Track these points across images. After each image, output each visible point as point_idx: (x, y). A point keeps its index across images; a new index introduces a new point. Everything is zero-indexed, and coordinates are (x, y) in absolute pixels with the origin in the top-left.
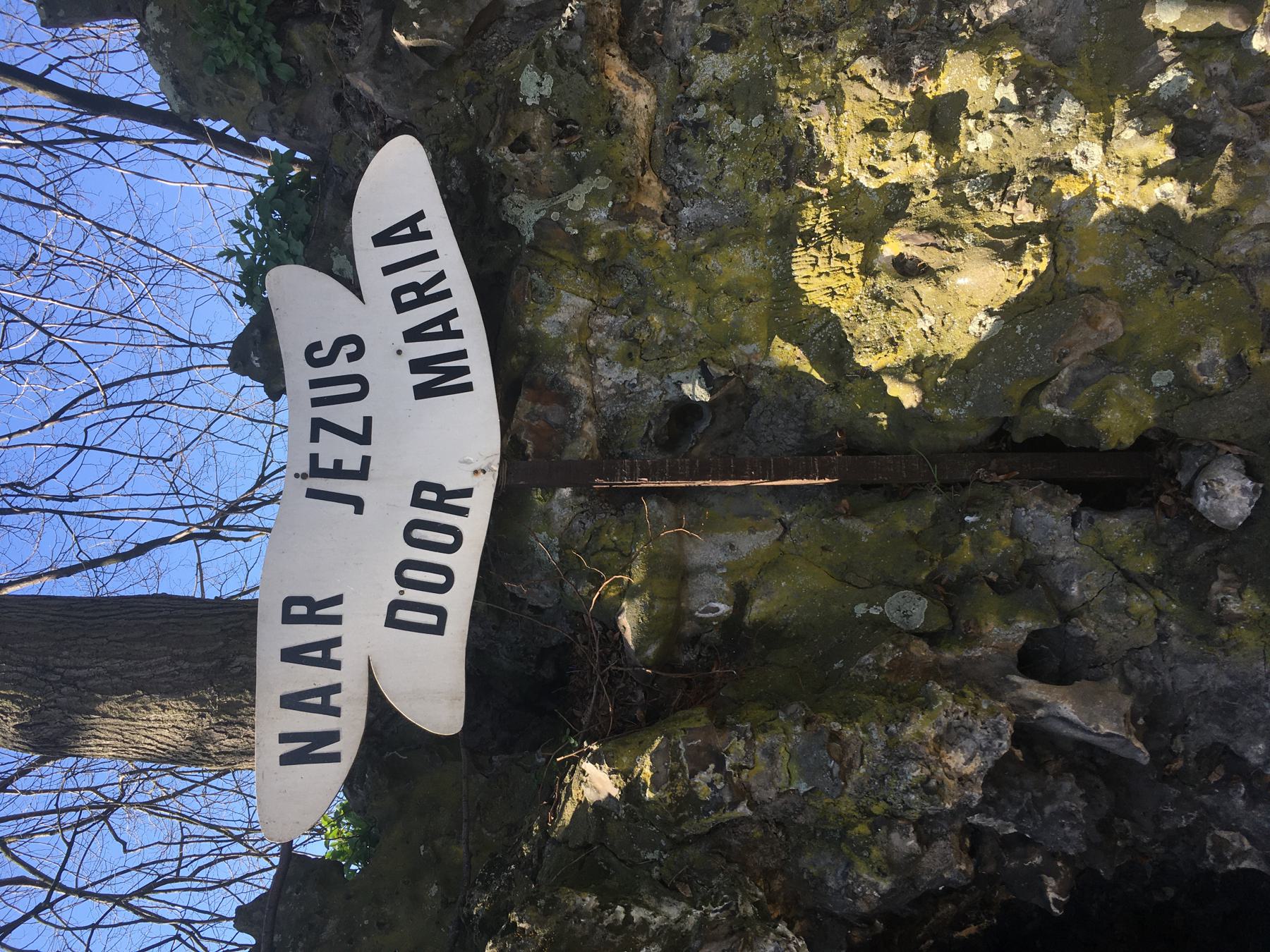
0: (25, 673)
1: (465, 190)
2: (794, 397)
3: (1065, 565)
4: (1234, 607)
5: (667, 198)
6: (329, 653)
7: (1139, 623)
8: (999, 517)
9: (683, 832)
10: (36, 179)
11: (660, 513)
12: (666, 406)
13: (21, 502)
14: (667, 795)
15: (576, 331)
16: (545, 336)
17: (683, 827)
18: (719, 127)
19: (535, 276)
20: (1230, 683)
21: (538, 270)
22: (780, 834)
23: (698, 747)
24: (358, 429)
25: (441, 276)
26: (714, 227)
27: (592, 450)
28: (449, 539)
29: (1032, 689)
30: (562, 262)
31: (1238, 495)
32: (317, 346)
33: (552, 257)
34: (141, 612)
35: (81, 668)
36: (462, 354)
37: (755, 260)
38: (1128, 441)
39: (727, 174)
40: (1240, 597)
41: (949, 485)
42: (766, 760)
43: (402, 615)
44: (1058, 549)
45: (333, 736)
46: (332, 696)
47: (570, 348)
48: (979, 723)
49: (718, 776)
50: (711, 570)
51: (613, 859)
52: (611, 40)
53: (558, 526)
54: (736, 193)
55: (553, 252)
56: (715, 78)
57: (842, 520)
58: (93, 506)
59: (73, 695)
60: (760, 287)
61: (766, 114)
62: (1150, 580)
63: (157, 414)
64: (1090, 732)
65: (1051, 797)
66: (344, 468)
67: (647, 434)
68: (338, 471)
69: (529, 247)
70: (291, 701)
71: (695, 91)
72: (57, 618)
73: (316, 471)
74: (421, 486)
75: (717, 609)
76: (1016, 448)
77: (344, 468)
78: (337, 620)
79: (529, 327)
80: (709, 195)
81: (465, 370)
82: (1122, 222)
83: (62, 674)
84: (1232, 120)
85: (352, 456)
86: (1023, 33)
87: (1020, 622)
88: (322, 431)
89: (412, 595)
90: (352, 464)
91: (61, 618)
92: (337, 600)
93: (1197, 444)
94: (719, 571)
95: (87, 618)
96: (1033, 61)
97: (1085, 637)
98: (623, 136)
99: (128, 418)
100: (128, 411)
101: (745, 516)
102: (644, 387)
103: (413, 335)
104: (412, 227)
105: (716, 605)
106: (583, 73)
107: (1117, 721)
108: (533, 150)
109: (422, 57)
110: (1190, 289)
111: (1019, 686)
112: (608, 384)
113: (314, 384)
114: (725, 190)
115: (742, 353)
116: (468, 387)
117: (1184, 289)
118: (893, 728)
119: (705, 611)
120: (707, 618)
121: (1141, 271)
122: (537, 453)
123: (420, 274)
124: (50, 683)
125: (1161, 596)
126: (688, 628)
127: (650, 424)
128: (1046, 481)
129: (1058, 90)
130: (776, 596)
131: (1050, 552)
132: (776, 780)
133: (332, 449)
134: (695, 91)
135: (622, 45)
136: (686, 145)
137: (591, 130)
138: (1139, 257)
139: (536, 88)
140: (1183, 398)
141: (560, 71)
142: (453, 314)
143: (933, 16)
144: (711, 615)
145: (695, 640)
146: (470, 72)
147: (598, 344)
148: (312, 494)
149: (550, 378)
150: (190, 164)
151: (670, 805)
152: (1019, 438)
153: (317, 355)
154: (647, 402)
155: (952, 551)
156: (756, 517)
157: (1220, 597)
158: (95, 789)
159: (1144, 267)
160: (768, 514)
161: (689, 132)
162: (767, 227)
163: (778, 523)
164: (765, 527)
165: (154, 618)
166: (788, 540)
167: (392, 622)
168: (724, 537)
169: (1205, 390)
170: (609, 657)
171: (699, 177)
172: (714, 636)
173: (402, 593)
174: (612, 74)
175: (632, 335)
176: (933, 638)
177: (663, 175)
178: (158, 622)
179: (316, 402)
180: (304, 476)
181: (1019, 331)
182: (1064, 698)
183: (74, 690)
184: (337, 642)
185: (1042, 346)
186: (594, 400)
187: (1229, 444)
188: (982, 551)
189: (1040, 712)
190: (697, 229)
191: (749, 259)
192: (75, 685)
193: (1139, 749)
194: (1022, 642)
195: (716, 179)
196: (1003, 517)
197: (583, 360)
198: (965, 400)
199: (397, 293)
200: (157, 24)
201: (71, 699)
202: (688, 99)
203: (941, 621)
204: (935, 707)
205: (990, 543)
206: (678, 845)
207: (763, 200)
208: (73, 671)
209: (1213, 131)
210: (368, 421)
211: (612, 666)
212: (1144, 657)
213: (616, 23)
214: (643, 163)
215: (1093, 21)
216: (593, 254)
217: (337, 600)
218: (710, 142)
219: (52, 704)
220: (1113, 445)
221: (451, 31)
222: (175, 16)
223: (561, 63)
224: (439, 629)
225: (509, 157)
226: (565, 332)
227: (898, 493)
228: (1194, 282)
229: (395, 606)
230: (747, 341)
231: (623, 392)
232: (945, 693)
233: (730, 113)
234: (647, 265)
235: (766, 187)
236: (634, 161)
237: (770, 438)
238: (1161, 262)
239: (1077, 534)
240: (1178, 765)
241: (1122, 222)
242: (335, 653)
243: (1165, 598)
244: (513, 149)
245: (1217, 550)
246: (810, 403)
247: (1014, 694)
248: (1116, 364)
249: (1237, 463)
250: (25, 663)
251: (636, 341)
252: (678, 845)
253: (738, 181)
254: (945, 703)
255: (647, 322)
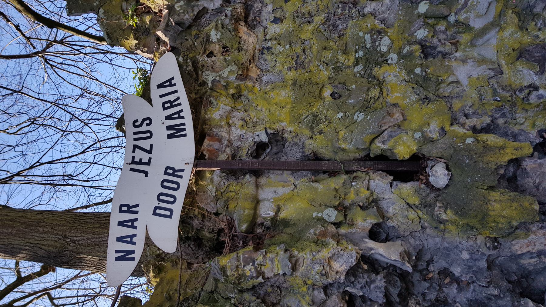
0: (58, 238)
1: (192, 70)
2: (299, 141)
3: (387, 201)
4: (444, 217)
5: (259, 73)
6: (133, 224)
7: (413, 222)
8: (363, 183)
9: (242, 287)
10: (82, 65)
11: (250, 180)
12: (255, 143)
13: (70, 182)
14: (236, 273)
15: (225, 117)
16: (214, 119)
17: (242, 286)
18: (275, 49)
19: (212, 99)
20: (447, 245)
21: (213, 97)
22: (278, 291)
23: (247, 258)
24: (148, 149)
25: (178, 98)
26: (273, 82)
27: (228, 158)
28: (175, 186)
29: (371, 244)
30: (221, 94)
31: (442, 176)
32: (137, 121)
33: (218, 92)
34: (100, 218)
35: (77, 237)
36: (184, 124)
37: (286, 94)
38: (407, 157)
39: (277, 65)
40: (445, 213)
41: (349, 172)
42: (270, 263)
43: (158, 211)
44: (385, 195)
45: (133, 252)
46: (133, 238)
47: (223, 123)
48: (346, 253)
49: (253, 267)
50: (268, 200)
51: (220, 296)
52: (241, 20)
53: (216, 183)
54: (281, 71)
55: (218, 91)
56: (275, 32)
57: (312, 183)
58: (95, 184)
59: (74, 246)
60: (287, 103)
61: (290, 44)
62: (417, 207)
63: (119, 151)
64: (388, 259)
65: (373, 281)
66: (143, 161)
67: (248, 153)
68: (141, 162)
69: (210, 89)
70: (120, 239)
71: (268, 37)
72: (70, 219)
73: (133, 162)
74: (167, 168)
75: (269, 214)
76: (371, 159)
77: (143, 161)
78: (137, 212)
79: (209, 116)
80: (271, 72)
81: (184, 130)
82: (406, 81)
83: (71, 239)
84: (444, 46)
85: (145, 157)
86: (375, 17)
87: (368, 220)
88: (136, 149)
89: (162, 205)
90: (145, 160)
91: (72, 219)
92: (137, 206)
93: (431, 158)
94: (271, 200)
95: (81, 219)
96: (377, 26)
97: (393, 226)
98: (243, 52)
99: (109, 152)
100: (109, 149)
101: (281, 182)
102: (247, 137)
103: (168, 118)
104: (170, 82)
105: (269, 212)
106: (230, 31)
107: (397, 255)
108: (215, 56)
109: (180, 26)
110: (428, 104)
111: (367, 243)
112: (235, 135)
113: (135, 133)
114: (276, 70)
115: (281, 126)
116: (185, 135)
117: (426, 104)
118: (314, 253)
119: (265, 214)
120: (266, 217)
121: (411, 98)
122: (209, 158)
123: (171, 98)
124: (67, 242)
125: (420, 213)
126: (259, 220)
127: (249, 149)
128: (382, 171)
129: (384, 36)
130: (289, 210)
131: (383, 196)
132: (273, 270)
133: (139, 155)
134: (268, 37)
135: (246, 22)
136: (265, 55)
137: (233, 50)
138: (411, 93)
139: (216, 36)
140: (424, 142)
141: (222, 31)
142: (182, 111)
143: (347, 11)
144: (267, 216)
145: (262, 224)
146: (196, 31)
147: (233, 122)
148: (132, 170)
149: (215, 133)
150: (135, 61)
151: (236, 277)
152: (372, 156)
153: (137, 124)
154: (248, 142)
155: (347, 195)
156: (285, 182)
157: (438, 213)
158: (93, 289)
159: (413, 96)
160: (290, 181)
161: (266, 50)
162: (290, 82)
163: (293, 185)
164: (288, 186)
165: (104, 220)
166: (295, 190)
167: (155, 214)
168: (273, 189)
169: (431, 139)
170: (232, 229)
171: (268, 66)
172: (268, 223)
173: (159, 204)
174: (241, 31)
175: (244, 119)
176: (337, 225)
177: (257, 65)
178: (105, 222)
179: (135, 139)
180: (130, 164)
181: (368, 118)
182: (381, 247)
183: (74, 245)
184: (136, 220)
185: (375, 123)
186: (229, 141)
187: (440, 158)
188: (358, 195)
189: (372, 252)
190: (267, 83)
191: (284, 93)
192: (75, 243)
193: (408, 267)
194: (370, 227)
195: (274, 66)
196: (364, 183)
197: (227, 127)
198: (351, 142)
199: (164, 104)
200: (102, 15)
201: (73, 248)
202: (266, 40)
203: (341, 218)
204: (329, 247)
205: (360, 192)
206: (241, 291)
207: (289, 73)
208: (75, 238)
209: (437, 50)
210: (151, 146)
211: (233, 232)
212: (417, 235)
213: (243, 14)
214: (250, 61)
215: (400, 12)
216: (231, 91)
217: (137, 206)
218: (272, 54)
219: (67, 249)
220: (401, 158)
221: (188, 18)
222: (108, 12)
223: (223, 28)
224: (170, 217)
225: (206, 59)
226: (221, 117)
227: (333, 174)
228: (429, 101)
229: (156, 208)
230: (282, 122)
231: (241, 138)
232: (333, 242)
233: (279, 44)
234: (250, 96)
235: (290, 69)
236: (246, 60)
237: (292, 155)
238: (419, 95)
239: (392, 190)
240: (431, 275)
241: (406, 81)
242: (135, 224)
243: (422, 213)
244: (208, 56)
245: (438, 196)
246: (304, 143)
247: (365, 245)
248: (403, 130)
249: (444, 165)
250: (58, 234)
251: (245, 121)
252: (241, 291)
253: (281, 67)
254: (333, 245)
255: (249, 115)
